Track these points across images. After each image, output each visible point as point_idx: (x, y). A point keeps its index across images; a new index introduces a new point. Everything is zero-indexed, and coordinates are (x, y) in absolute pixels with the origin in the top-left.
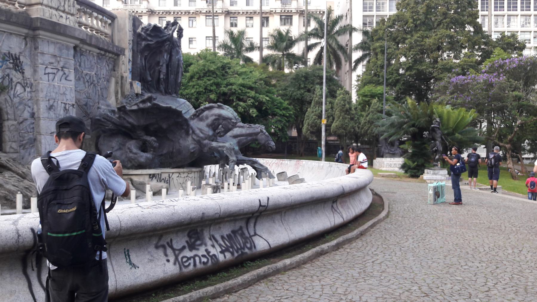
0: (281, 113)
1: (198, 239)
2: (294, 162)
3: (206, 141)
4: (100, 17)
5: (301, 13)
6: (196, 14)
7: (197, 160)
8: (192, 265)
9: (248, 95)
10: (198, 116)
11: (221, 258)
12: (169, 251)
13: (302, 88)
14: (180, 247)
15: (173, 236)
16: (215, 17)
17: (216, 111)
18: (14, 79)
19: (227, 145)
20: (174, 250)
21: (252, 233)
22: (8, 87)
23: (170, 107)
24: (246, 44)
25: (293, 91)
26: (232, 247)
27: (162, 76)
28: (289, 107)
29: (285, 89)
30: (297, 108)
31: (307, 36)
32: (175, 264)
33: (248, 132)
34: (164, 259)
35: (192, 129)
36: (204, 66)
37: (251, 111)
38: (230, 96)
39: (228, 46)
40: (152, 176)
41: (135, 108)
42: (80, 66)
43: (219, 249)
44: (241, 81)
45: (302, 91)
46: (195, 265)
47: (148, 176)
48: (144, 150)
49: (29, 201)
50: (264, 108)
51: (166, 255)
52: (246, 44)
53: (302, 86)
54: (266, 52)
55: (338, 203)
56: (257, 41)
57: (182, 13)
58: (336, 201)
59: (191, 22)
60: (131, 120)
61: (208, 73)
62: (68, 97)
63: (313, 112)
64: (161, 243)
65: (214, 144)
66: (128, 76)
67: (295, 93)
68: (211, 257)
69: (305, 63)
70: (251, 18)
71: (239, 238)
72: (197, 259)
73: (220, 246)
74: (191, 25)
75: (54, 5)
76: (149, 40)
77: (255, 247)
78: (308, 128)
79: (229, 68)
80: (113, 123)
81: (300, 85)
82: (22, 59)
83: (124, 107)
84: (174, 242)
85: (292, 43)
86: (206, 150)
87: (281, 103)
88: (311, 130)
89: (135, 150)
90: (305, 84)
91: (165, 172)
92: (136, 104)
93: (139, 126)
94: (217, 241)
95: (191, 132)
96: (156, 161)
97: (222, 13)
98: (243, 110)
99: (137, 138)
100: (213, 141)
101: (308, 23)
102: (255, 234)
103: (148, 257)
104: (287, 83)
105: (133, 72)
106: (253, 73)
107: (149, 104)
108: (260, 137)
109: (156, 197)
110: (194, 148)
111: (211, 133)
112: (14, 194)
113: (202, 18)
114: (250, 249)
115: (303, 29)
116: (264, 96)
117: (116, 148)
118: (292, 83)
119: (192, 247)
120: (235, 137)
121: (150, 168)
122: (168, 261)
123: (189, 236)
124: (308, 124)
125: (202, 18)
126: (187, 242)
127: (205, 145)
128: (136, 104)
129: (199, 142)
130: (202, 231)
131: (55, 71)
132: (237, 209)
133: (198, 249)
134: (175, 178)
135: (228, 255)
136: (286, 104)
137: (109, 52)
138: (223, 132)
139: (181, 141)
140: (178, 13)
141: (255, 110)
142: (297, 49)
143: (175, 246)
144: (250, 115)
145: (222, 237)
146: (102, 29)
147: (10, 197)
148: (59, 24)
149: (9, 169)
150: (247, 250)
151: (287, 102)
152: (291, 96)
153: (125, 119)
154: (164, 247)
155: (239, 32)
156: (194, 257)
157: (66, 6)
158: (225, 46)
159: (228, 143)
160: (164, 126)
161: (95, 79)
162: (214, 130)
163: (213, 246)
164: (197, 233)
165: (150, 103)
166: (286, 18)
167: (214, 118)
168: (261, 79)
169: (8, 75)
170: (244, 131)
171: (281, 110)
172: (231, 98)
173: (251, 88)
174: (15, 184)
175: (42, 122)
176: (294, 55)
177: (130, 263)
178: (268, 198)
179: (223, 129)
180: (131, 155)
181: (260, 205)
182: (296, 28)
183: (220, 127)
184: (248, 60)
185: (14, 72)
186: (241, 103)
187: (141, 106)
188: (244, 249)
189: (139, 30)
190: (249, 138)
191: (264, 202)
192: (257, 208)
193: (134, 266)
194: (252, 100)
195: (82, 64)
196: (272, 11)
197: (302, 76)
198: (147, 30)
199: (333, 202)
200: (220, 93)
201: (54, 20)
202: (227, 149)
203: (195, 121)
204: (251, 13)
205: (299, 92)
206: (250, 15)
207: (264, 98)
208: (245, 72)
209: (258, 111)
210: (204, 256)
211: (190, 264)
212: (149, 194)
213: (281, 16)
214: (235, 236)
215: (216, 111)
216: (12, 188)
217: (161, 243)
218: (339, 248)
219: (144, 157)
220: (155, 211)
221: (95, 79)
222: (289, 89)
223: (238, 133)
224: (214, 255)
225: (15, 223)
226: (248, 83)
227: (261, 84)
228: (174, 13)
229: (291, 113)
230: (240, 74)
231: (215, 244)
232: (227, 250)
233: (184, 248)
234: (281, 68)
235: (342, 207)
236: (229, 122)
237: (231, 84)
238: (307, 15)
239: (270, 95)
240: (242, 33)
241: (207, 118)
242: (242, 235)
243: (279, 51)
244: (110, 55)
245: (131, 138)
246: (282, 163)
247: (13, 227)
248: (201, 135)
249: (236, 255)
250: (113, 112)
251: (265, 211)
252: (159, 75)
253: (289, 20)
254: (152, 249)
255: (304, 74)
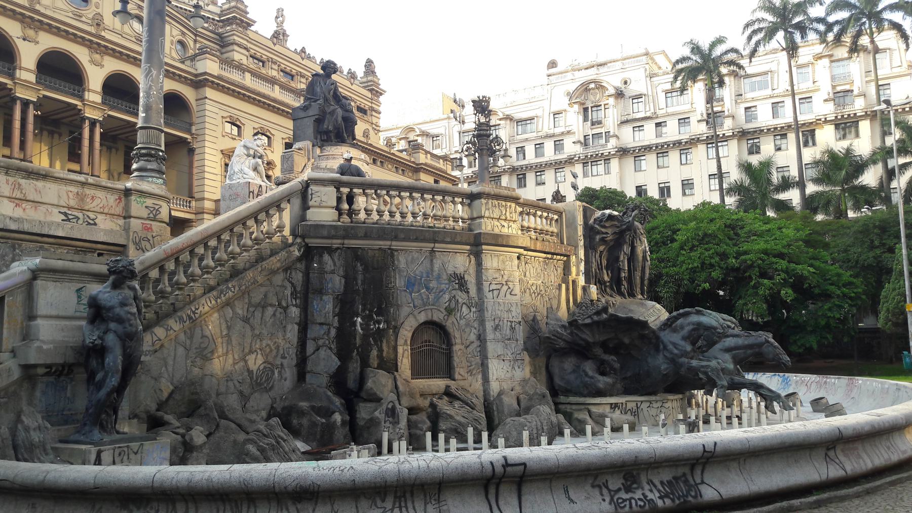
0: (838, 292)
1: (634, 482)
2: (844, 380)
3: (684, 360)
4: (545, 214)
5: (872, 116)
6: (691, 143)
7: (680, 383)
8: (628, 506)
9: (775, 266)
10: (670, 326)
11: (660, 503)
12: (605, 491)
13: (877, 247)
14: (616, 488)
15: (609, 478)
16: (719, 144)
17: (694, 318)
18: (460, 300)
19: (713, 363)
20: (609, 490)
21: (698, 481)
22: (454, 309)
23: (631, 318)
24: (775, 178)
25: (860, 254)
26: (673, 494)
27: (623, 275)
28: (855, 280)
29: (846, 251)
30: (872, 281)
31: (883, 154)
32: (610, 504)
33: (746, 343)
34: (600, 498)
35: (663, 342)
36: (698, 229)
37: (783, 292)
38: (745, 272)
39: (745, 188)
40: (614, 406)
41: (588, 321)
42: (525, 276)
43: (657, 495)
44: (762, 245)
45: (878, 252)
46: (631, 507)
47: (609, 406)
48: (603, 374)
49: (481, 435)
50: (806, 286)
51: (602, 495)
52: (775, 178)
53: (876, 243)
54: (811, 188)
55: (838, 452)
56: (794, 172)
57: (668, 145)
58: (834, 448)
59: (683, 157)
60: (584, 336)
61: (705, 239)
62: (514, 314)
63: (894, 290)
64: (597, 483)
65: (694, 363)
66: (581, 281)
67: (864, 257)
68: (649, 501)
69: (887, 200)
70: (784, 136)
71: (682, 485)
72: (633, 501)
73: (659, 491)
74: (684, 161)
75: (495, 216)
76: (603, 233)
77: (701, 496)
78: (887, 317)
79: (742, 228)
80: (564, 340)
81: (872, 241)
82: (466, 277)
83: (576, 320)
84: (609, 483)
85: (860, 167)
86: (683, 371)
87: (839, 275)
88: (894, 320)
89: (590, 373)
90: (882, 239)
91: (630, 401)
92: (590, 317)
93: (594, 343)
94: (655, 486)
95: (661, 347)
96: (619, 386)
97: (733, 136)
98: (767, 292)
99: (594, 358)
100: (692, 358)
101: (885, 133)
102: (703, 482)
103: (585, 494)
104: (848, 240)
105: (587, 274)
106: (784, 230)
107: (605, 316)
108: (765, 349)
109: (615, 435)
110: (667, 369)
111: (689, 348)
112: (465, 427)
113: (702, 148)
114: (695, 497)
115: (878, 144)
116: (805, 266)
117: (569, 371)
118: (856, 238)
119: (628, 490)
120: (728, 350)
121: (611, 395)
122: (604, 500)
123: (624, 478)
124: (888, 310)
125: (702, 148)
126: (623, 484)
127: (681, 365)
128: (590, 317)
129: (673, 361)
130: (639, 474)
131: (498, 287)
132: (675, 454)
133: (634, 492)
134: (645, 410)
135: (668, 502)
136: (847, 276)
137: (557, 254)
138: (705, 346)
139: (649, 360)
140: (662, 146)
141: (790, 291)
142: (870, 178)
143: (610, 487)
144: (781, 299)
145: (662, 483)
146: (547, 228)
147: (461, 429)
148: (501, 236)
149: (458, 399)
150: (690, 499)
151: (849, 273)
152: (857, 262)
153: (577, 335)
154: (599, 487)
155: (761, 163)
156: (630, 500)
157: (508, 214)
158: (737, 189)
159: (720, 360)
160: (626, 341)
161: (542, 288)
162: (693, 343)
163: (651, 491)
164: (633, 476)
165: (606, 314)
166: (846, 125)
167: (691, 327)
168: (797, 240)
169: (454, 297)
170: (740, 341)
171: (839, 288)
172: (747, 274)
173: (781, 256)
174: (465, 415)
175: (488, 344)
176: (864, 189)
177: (569, 499)
178: (715, 443)
179: (705, 343)
180: (587, 379)
181: (705, 451)
182: (864, 143)
183: (703, 339)
184: (783, 207)
185: (460, 293)
186: (766, 281)
187: (595, 318)
188: (687, 496)
189: (591, 221)
190: (749, 352)
191: (710, 447)
192: (700, 454)
193: (572, 501)
194: (783, 275)
195: (528, 273)
196: (820, 120)
197: (875, 227)
198: (601, 221)
199: (828, 449)
200: (727, 268)
201: (496, 231)
202: (713, 370)
203: (667, 332)
204: (782, 128)
205: (871, 254)
206: (780, 133)
207: (804, 269)
208: (769, 230)
209: (795, 292)
210: (639, 499)
211: (625, 506)
212: (607, 430)
213: (836, 125)
214: (677, 482)
215: (694, 318)
216: (463, 420)
217: (597, 483)
218: (820, 506)
219: (603, 381)
220: (588, 451)
221: (542, 288)
222: (853, 250)
223: (733, 345)
224: (652, 500)
225: (479, 456)
226: (775, 247)
227: (798, 247)
228: (657, 147)
229: (860, 290)
230: (760, 235)
231: (654, 489)
232: (667, 496)
233: (619, 489)
234: (841, 214)
235: (846, 456)
236: (713, 333)
237: (746, 253)
238: (881, 119)
239: (817, 263)
240: (766, 165)
241: (682, 328)
242: (686, 482)
243: (835, 185)
244: (559, 257)
245: (587, 358)
246: (825, 382)
247: (478, 460)
248: (676, 351)
249: (677, 502)
250: (563, 326)
251: (712, 457)
252: (619, 274)
253: (853, 130)
254: (588, 487)
255: (877, 224)
